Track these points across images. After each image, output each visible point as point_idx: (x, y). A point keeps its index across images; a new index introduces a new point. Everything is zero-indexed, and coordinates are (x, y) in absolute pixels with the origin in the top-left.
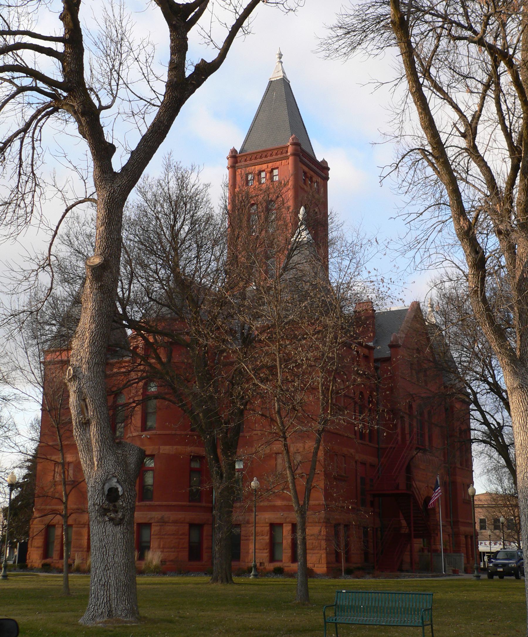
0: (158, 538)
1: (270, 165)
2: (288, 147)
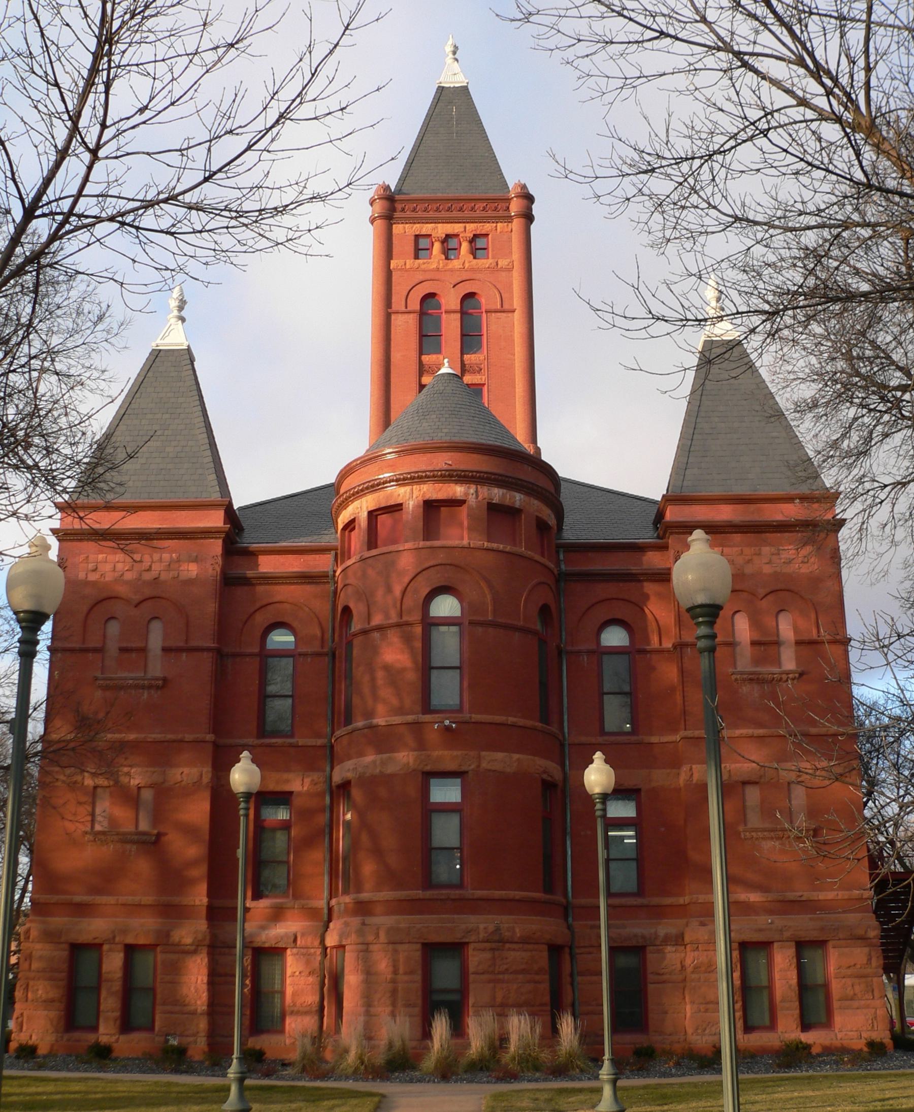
0: (490, 981)
1: (471, 227)
2: (509, 200)
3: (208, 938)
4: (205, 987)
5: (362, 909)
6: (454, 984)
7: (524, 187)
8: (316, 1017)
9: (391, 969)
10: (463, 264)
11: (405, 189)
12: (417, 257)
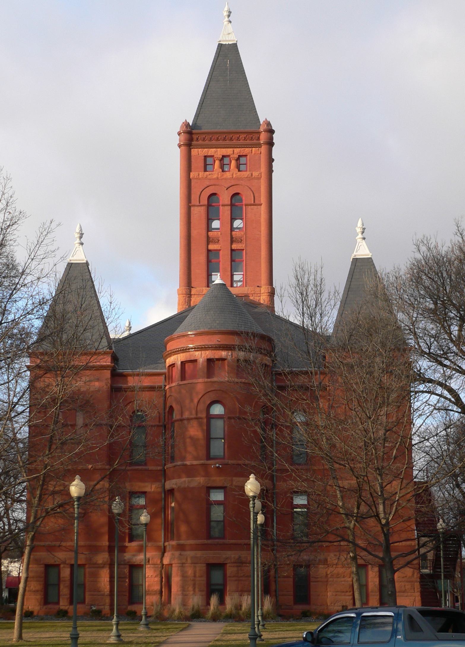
0: (236, 580)
1: (237, 150)
2: (259, 133)
3: (109, 560)
4: (108, 583)
5: (181, 548)
6: (220, 581)
7: (268, 124)
8: (159, 596)
9: (193, 575)
10: (233, 175)
11: (199, 123)
12: (205, 170)
